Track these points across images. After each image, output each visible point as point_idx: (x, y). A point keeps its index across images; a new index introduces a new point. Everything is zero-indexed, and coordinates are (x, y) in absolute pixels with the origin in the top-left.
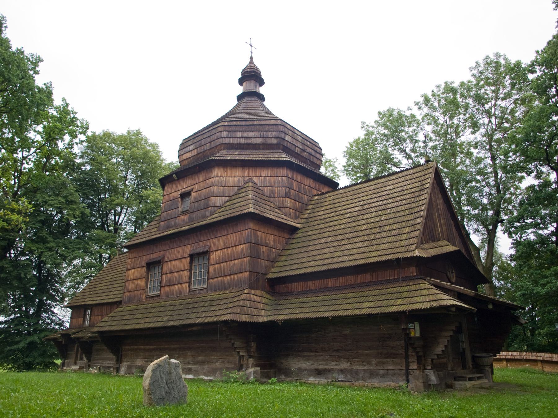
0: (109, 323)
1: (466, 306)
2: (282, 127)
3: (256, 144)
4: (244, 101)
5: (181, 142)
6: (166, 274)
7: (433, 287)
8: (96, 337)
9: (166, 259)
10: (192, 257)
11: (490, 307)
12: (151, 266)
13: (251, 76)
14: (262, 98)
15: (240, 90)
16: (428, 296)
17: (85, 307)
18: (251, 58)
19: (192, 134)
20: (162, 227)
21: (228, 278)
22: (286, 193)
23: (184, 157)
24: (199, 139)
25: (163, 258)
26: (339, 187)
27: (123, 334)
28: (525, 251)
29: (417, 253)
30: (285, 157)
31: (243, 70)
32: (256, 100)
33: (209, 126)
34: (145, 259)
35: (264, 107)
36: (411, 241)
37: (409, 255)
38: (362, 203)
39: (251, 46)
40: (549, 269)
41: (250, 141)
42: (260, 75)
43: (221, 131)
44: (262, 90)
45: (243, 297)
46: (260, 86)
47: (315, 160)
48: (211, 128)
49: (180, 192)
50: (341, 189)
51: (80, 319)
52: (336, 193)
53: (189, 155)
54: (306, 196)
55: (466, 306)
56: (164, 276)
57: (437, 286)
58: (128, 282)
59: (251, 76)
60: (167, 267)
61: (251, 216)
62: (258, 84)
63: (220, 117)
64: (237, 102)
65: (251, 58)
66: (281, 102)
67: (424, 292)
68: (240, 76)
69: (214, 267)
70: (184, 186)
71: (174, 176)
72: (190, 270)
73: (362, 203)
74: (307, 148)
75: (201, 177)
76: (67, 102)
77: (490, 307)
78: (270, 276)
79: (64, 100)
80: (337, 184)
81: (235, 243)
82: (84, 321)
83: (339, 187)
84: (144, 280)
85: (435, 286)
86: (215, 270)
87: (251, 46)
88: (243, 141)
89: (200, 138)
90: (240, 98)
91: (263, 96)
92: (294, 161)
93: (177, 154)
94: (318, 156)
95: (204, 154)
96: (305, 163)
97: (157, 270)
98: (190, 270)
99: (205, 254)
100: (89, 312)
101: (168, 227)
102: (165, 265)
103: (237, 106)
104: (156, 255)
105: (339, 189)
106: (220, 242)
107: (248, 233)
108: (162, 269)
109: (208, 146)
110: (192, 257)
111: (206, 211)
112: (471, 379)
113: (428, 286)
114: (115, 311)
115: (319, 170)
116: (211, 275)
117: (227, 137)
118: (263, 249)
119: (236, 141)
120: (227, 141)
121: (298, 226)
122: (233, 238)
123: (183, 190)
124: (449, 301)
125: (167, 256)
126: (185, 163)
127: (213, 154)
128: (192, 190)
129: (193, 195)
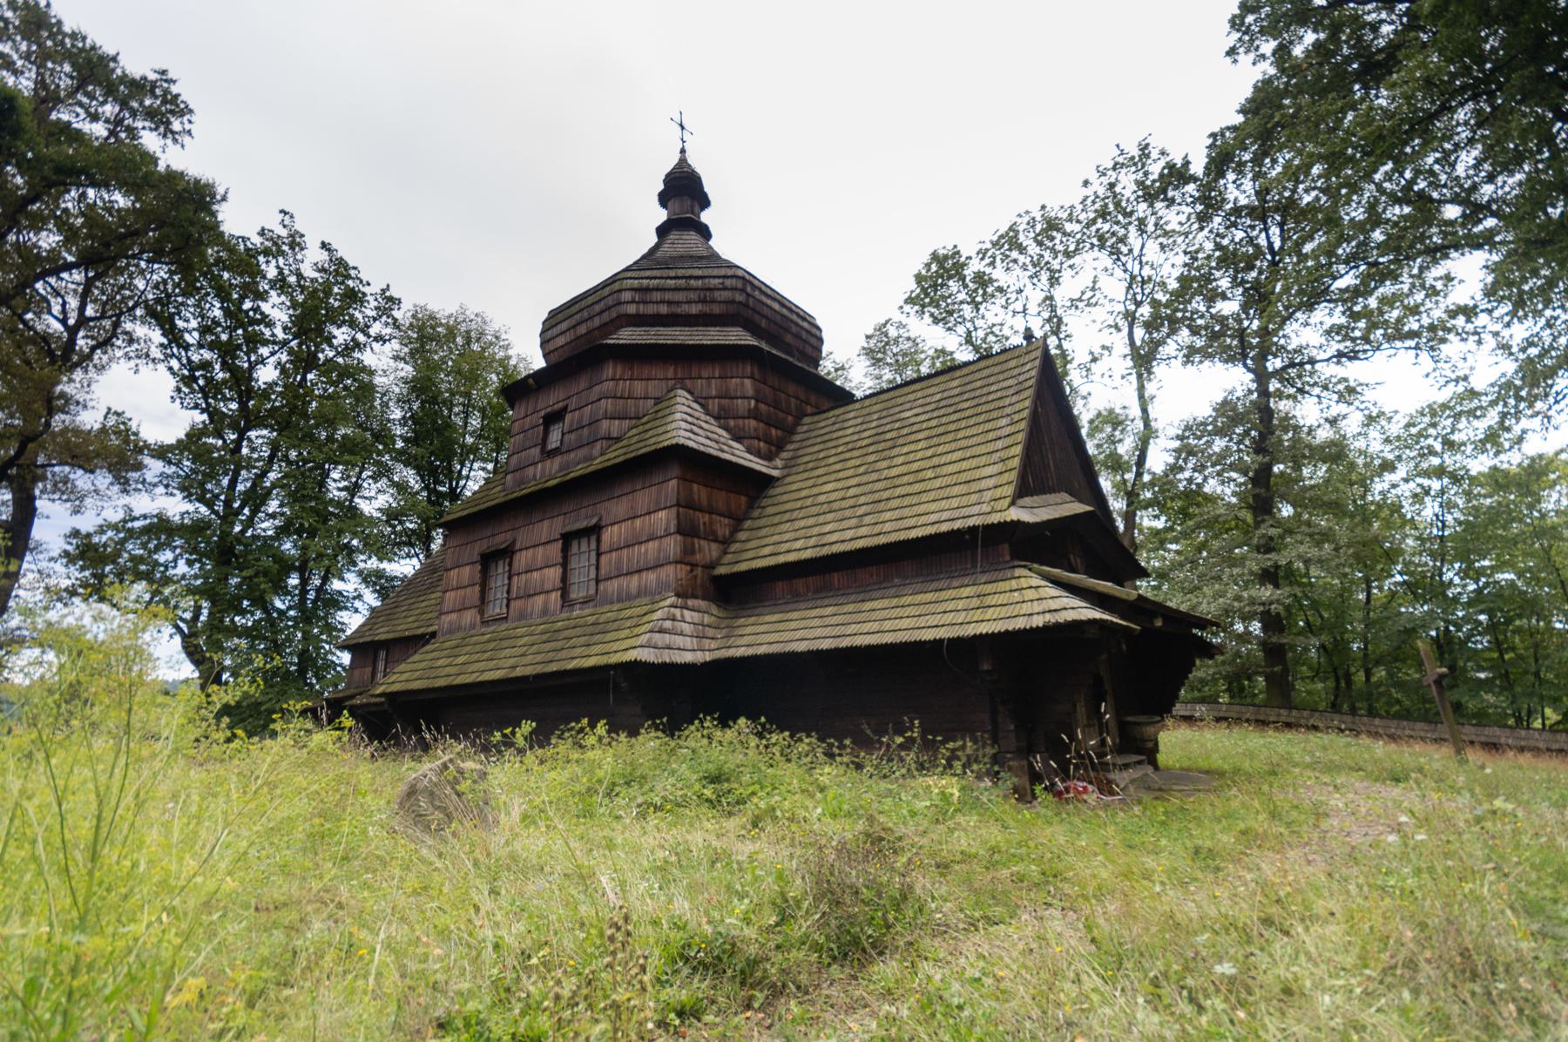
1: (1106, 617)
2: (746, 283)
4: (673, 236)
7: (1043, 583)
8: (381, 704)
9: (518, 546)
10: (568, 539)
11: (1159, 623)
12: (488, 560)
13: (684, 190)
14: (705, 233)
15: (662, 215)
16: (1034, 601)
18: (683, 151)
23: (552, 346)
25: (514, 542)
27: (432, 696)
28: (1282, 473)
29: (1014, 514)
30: (736, 336)
32: (692, 237)
35: (714, 257)
36: (998, 492)
38: (897, 425)
44: (706, 217)
45: (659, 615)
46: (703, 209)
47: (809, 350)
53: (561, 341)
56: (515, 579)
57: (1057, 583)
59: (684, 190)
61: (680, 454)
64: (655, 240)
65: (683, 151)
66: (739, 236)
67: (1030, 594)
68: (661, 187)
70: (551, 400)
72: (565, 564)
73: (897, 425)
76: (298, 227)
77: (1159, 623)
78: (722, 570)
84: (477, 588)
85: (1052, 582)
88: (664, 309)
90: (662, 231)
94: (813, 340)
95: (590, 337)
97: (502, 567)
98: (565, 564)
99: (595, 531)
100: (382, 654)
102: (517, 557)
104: (500, 540)
106: (618, 508)
110: (568, 539)
112: (1126, 766)
113: (1036, 581)
116: (603, 572)
119: (651, 309)
120: (632, 309)
121: (775, 473)
122: (643, 498)
128: (566, 408)
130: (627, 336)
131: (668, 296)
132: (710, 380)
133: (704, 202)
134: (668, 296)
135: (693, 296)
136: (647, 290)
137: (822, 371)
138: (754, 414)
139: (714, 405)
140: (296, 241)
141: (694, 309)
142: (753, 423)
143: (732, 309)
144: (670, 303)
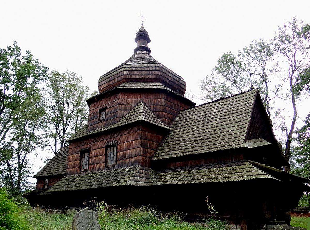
0: (57, 187)
1: (275, 179)
2: (162, 69)
3: (145, 79)
4: (139, 52)
5: (99, 78)
6: (92, 157)
13: (143, 36)
14: (149, 50)
15: (136, 45)
16: (251, 172)
17: (45, 177)
18: (142, 24)
19: (128, 59)
20: (88, 129)
21: (128, 160)
22: (163, 109)
23: (102, 87)
24: (110, 76)
25: (90, 148)
26: (196, 106)
30: (160, 86)
31: (138, 33)
32: (145, 52)
33: (116, 68)
34: (79, 149)
35: (150, 56)
37: (238, 146)
39: (142, 17)
40: (2, 51)
41: (141, 77)
42: (148, 36)
43: (124, 71)
44: (149, 45)
47: (181, 89)
48: (117, 69)
49: (99, 108)
50: (197, 106)
51: (42, 184)
52: (195, 108)
54: (175, 111)
55: (275, 179)
56: (91, 159)
58: (69, 162)
59: (143, 36)
60: (93, 153)
61: (142, 123)
62: (146, 42)
63: (123, 62)
65: (142, 24)
66: (163, 54)
68: (149, 37)
69: (120, 153)
71: (96, 98)
74: (177, 82)
75: (112, 99)
79: (28, 52)
80: (195, 104)
81: (132, 139)
82: (44, 186)
83: (196, 106)
84: (78, 161)
86: (120, 155)
87: (142, 17)
88: (137, 77)
89: (111, 75)
90: (136, 51)
91: (149, 49)
92: (168, 89)
93: (97, 86)
94: (183, 86)
96: (175, 91)
99: (116, 145)
100: (47, 180)
101: (92, 130)
102: (91, 152)
103: (134, 55)
104: (86, 146)
105: (196, 107)
106: (123, 138)
107: (140, 133)
108: (89, 154)
109: (116, 80)
111: (115, 120)
114: (61, 180)
115: (184, 95)
117: (127, 75)
118: (149, 142)
119: (133, 77)
120: (127, 77)
121: (171, 129)
122: (131, 135)
123: (101, 107)
124: (264, 175)
125: (92, 147)
126: (102, 91)
127: (119, 85)
129: (107, 110)
130: (126, 85)
131: (138, 73)
132: (151, 99)
133: (148, 40)
134: (138, 73)
135: (146, 73)
136: (132, 71)
137: (186, 96)
138: (164, 110)
139: (152, 107)
140: (18, 49)
141: (146, 77)
142: (164, 113)
143: (158, 77)
144: (139, 75)
